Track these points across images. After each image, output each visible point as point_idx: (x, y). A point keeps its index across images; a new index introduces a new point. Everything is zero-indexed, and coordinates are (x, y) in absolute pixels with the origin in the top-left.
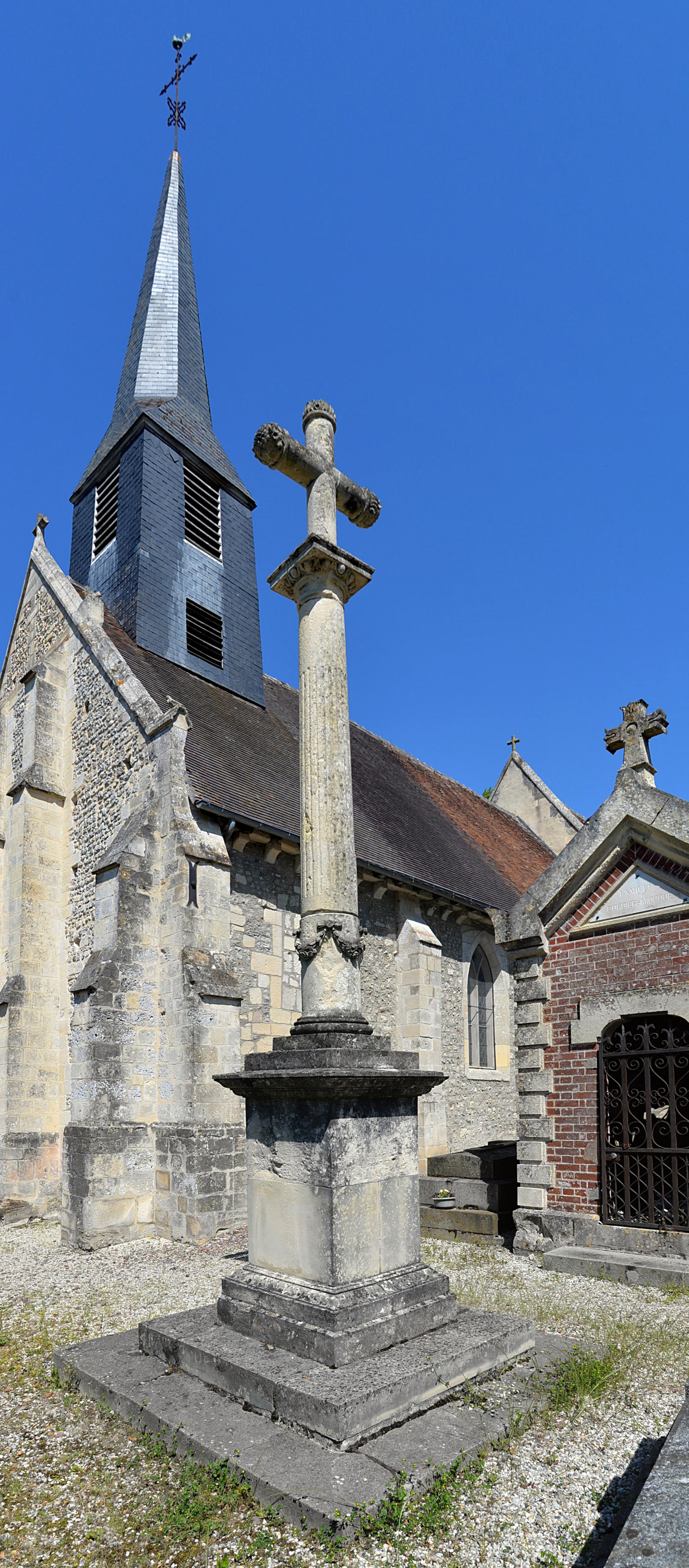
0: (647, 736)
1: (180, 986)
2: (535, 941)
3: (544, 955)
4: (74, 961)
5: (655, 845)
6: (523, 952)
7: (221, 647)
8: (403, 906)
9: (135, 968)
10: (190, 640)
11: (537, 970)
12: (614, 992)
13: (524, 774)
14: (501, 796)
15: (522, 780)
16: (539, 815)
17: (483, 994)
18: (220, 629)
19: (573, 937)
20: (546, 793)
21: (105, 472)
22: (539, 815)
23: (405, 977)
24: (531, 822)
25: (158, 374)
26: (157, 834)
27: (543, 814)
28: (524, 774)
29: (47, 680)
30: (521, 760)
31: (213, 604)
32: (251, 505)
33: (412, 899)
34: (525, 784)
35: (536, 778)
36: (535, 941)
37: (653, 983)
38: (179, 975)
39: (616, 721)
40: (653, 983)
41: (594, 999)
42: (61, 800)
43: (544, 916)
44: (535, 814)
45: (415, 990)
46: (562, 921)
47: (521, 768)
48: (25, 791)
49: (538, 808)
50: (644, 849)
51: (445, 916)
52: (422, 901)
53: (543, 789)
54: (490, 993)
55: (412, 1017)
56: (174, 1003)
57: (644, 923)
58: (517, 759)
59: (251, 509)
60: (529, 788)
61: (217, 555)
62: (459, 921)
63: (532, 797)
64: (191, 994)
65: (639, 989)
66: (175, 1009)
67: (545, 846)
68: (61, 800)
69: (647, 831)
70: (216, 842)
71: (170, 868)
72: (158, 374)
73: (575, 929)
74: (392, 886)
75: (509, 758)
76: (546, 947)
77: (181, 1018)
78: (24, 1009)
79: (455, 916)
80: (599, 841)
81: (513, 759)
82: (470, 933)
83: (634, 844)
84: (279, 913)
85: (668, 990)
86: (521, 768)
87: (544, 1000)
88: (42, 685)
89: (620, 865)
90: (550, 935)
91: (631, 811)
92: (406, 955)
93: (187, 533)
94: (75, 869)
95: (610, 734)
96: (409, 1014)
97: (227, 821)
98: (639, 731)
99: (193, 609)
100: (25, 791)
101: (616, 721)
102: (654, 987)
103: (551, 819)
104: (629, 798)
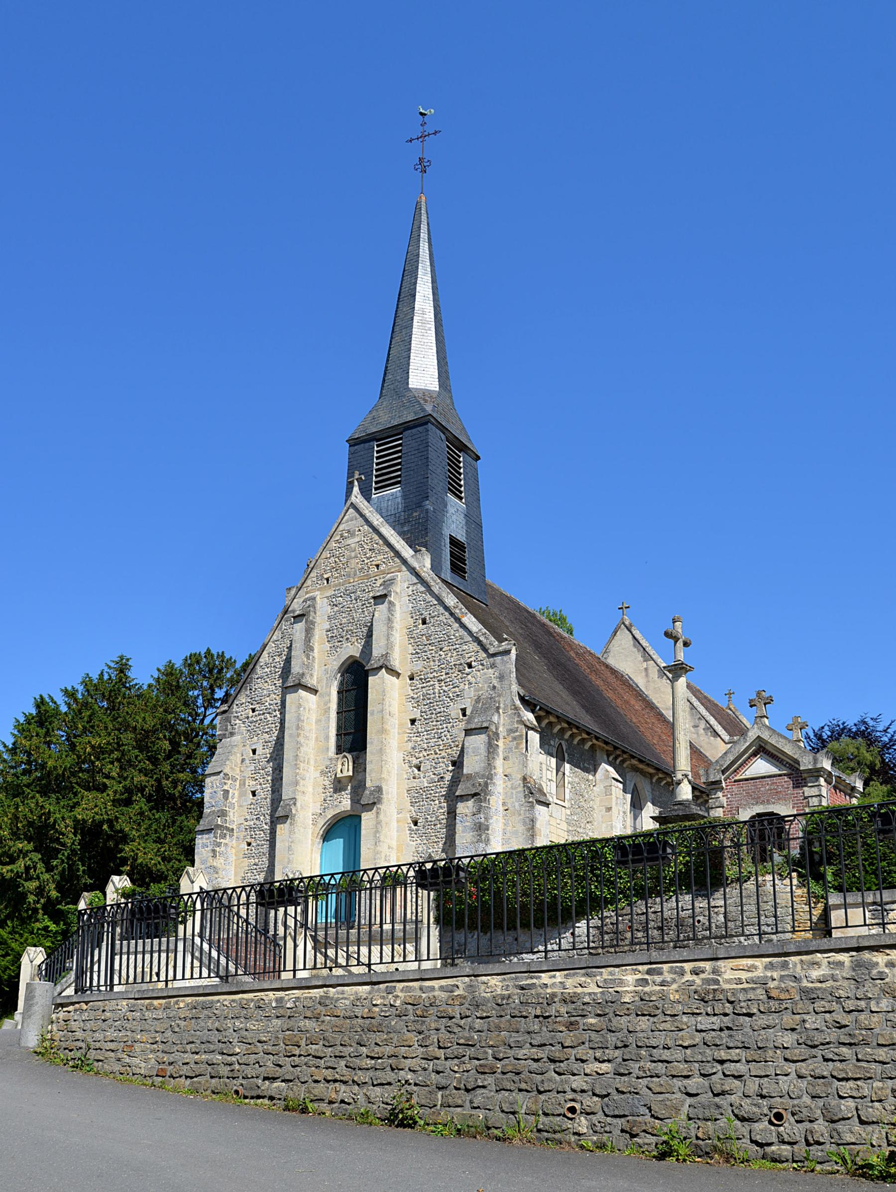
0: (765, 704)
1: (522, 795)
2: (719, 782)
3: (723, 788)
4: (414, 778)
5: (768, 747)
6: (713, 786)
7: (465, 564)
8: (598, 754)
9: (494, 784)
10: (452, 563)
11: (720, 794)
12: (753, 804)
13: (634, 637)
14: (611, 654)
15: (632, 643)
16: (647, 675)
17: (635, 818)
18: (465, 552)
19: (735, 781)
20: (654, 657)
21: (385, 435)
22: (647, 675)
23: (601, 801)
24: (640, 681)
25: (423, 374)
26: (501, 711)
27: (651, 675)
28: (634, 637)
29: (392, 599)
30: (631, 625)
31: (461, 537)
32: (478, 458)
33: (602, 749)
34: (635, 646)
35: (644, 643)
36: (719, 782)
37: (768, 801)
38: (521, 789)
39: (754, 696)
40: (768, 801)
41: (748, 805)
42: (398, 675)
43: (723, 772)
44: (644, 674)
45: (609, 809)
46: (730, 775)
47: (631, 632)
48: (384, 670)
49: (646, 669)
50: (765, 748)
51: (618, 761)
52: (607, 751)
53: (651, 653)
54: (640, 818)
55: (607, 827)
56: (517, 804)
57: (764, 777)
58: (627, 623)
59: (476, 460)
60: (639, 650)
61: (461, 498)
62: (625, 765)
63: (642, 659)
64: (531, 800)
65: (763, 803)
66: (517, 807)
67: (653, 703)
68: (398, 675)
69: (766, 742)
70: (529, 716)
71: (511, 731)
72: (423, 374)
73: (736, 778)
74: (595, 741)
75: (618, 621)
76: (724, 785)
77: (522, 812)
78: (382, 807)
79: (623, 761)
80: (748, 744)
81: (623, 623)
82: (630, 774)
83: (761, 746)
84: (545, 756)
85: (774, 803)
86: (631, 632)
87: (723, 807)
88: (390, 602)
89: (754, 754)
90: (725, 780)
91: (760, 734)
92: (602, 786)
93: (449, 489)
94: (413, 722)
95: (751, 701)
96: (604, 825)
97: (535, 706)
98: (762, 702)
99: (454, 542)
100: (384, 670)
101: (754, 696)
102: (768, 802)
103: (659, 680)
104: (759, 729)
